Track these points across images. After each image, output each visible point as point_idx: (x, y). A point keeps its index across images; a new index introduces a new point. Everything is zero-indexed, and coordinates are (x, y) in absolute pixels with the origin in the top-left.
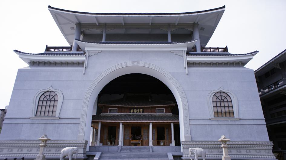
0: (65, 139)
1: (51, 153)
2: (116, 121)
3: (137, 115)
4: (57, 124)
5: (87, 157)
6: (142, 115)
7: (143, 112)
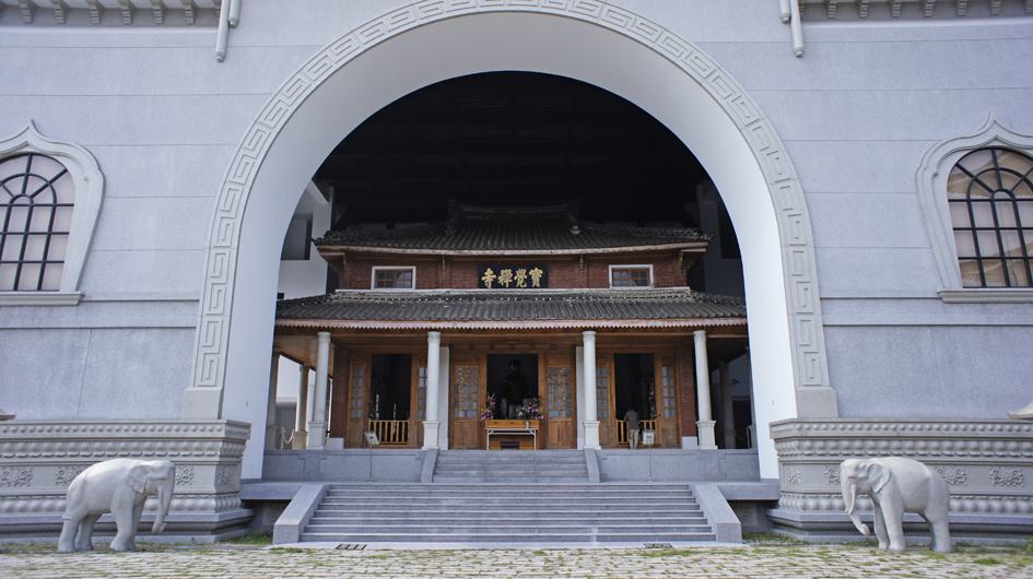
0: (113, 414)
1: (30, 497)
2: (410, 325)
3: (510, 297)
4: (69, 332)
5: (245, 513)
6: (540, 297)
7: (544, 283)
